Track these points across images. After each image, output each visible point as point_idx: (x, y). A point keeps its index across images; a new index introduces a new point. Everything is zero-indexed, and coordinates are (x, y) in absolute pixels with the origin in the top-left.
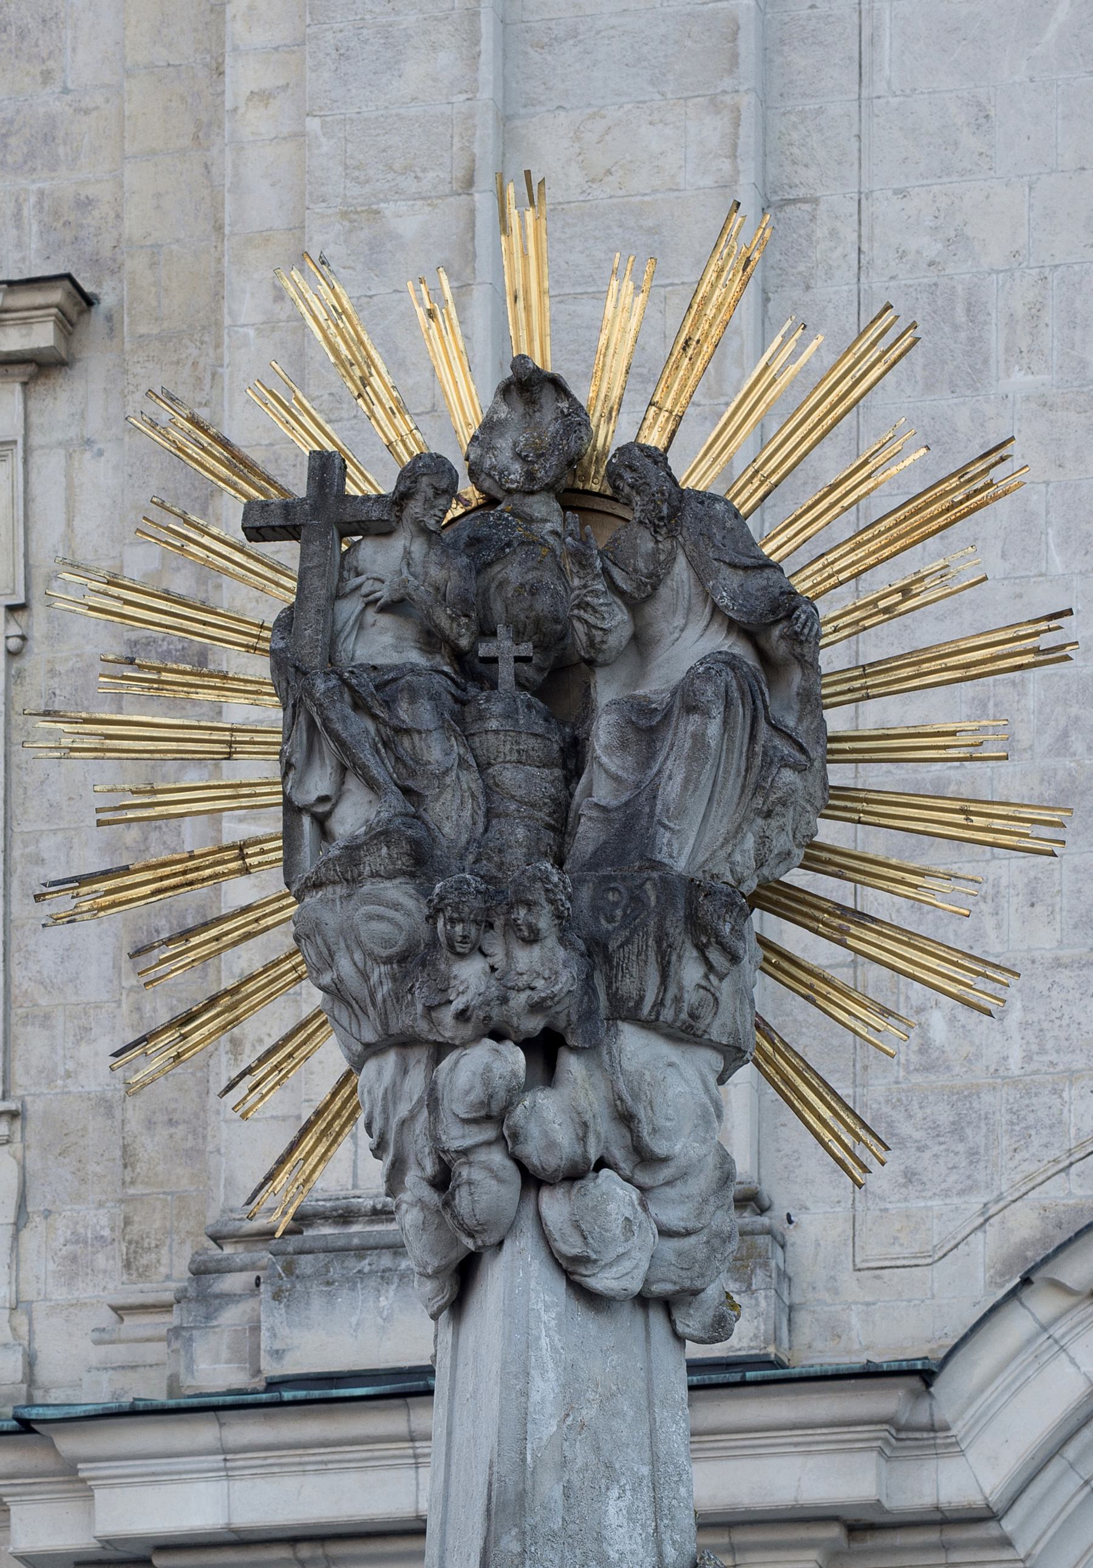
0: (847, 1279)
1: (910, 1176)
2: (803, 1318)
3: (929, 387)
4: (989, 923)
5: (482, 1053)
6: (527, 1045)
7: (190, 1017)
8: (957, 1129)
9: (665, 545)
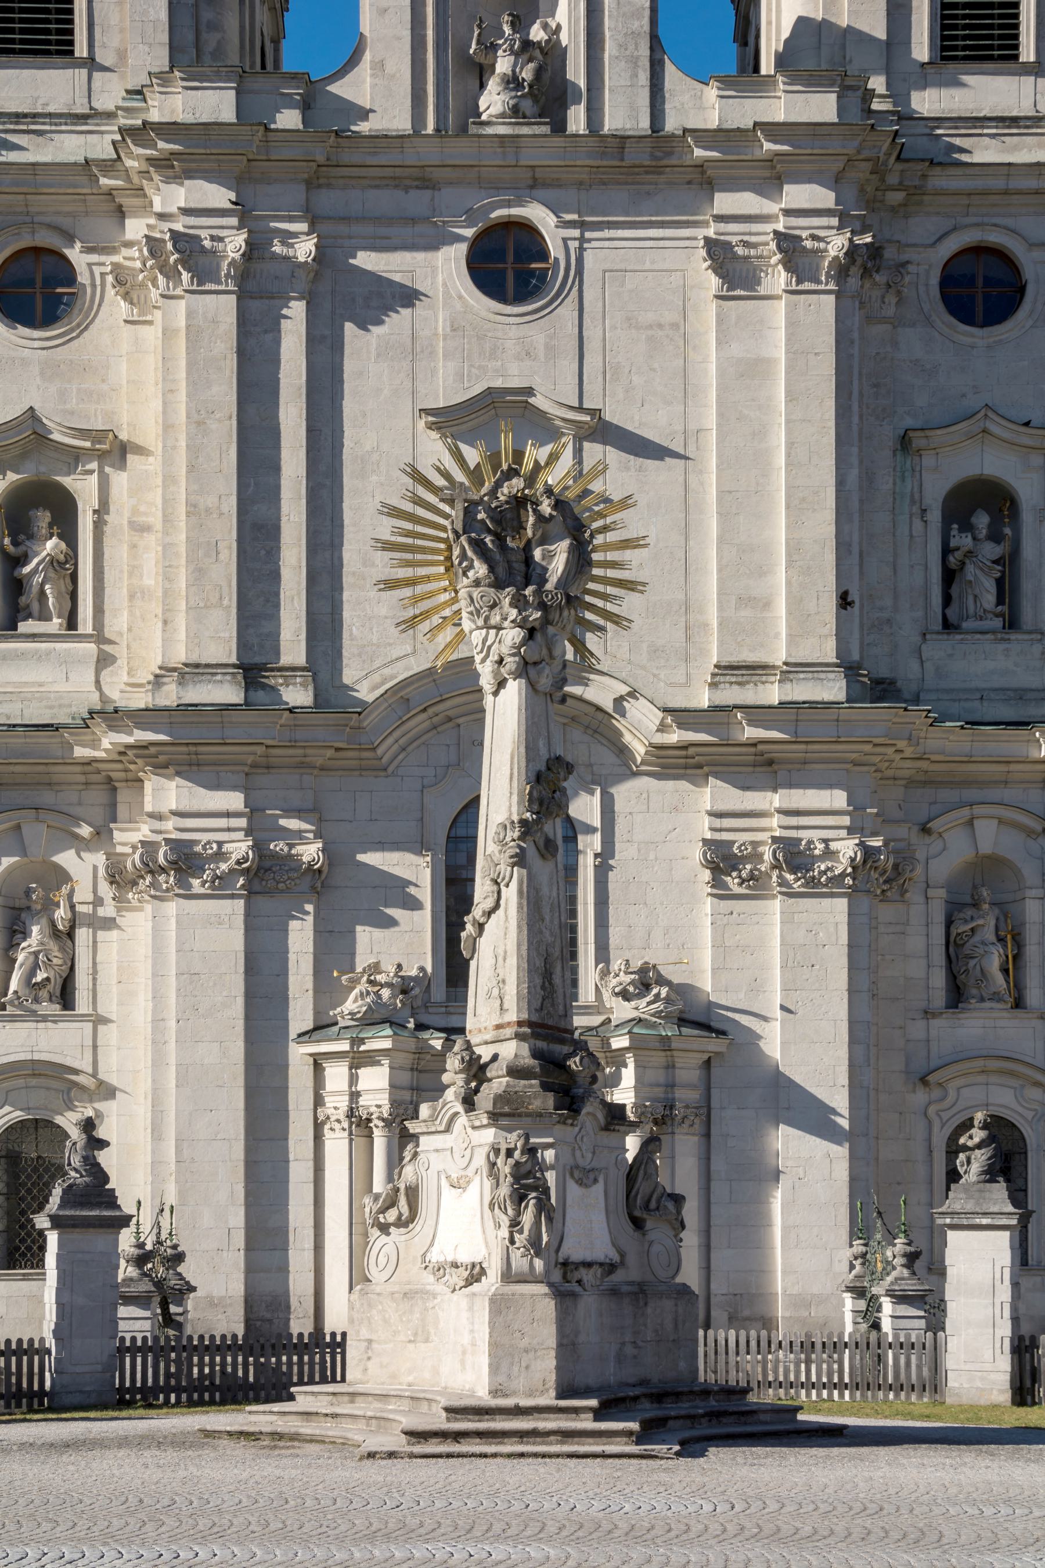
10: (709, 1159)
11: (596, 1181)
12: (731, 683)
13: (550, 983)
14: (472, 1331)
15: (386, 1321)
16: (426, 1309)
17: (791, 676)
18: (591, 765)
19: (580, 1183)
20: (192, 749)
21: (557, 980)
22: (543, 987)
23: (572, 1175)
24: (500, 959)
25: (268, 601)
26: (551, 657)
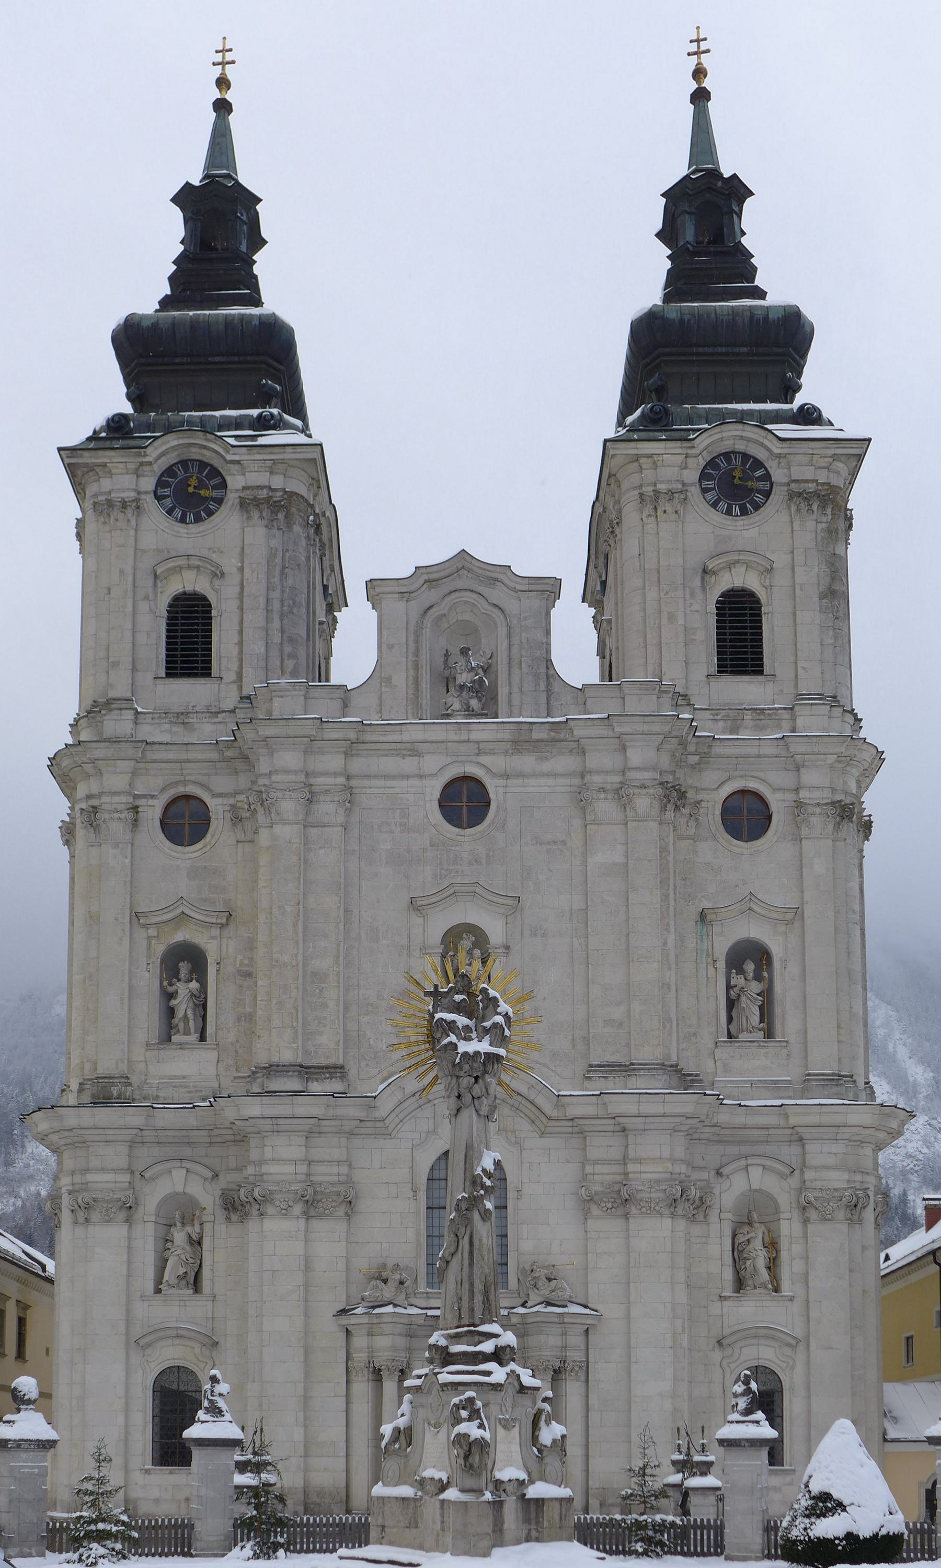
10: (587, 1396)
14: (442, 1522)
18: (515, 1131)
19: (505, 1427)
20: (275, 1121)
21: (492, 1298)
23: (500, 1423)
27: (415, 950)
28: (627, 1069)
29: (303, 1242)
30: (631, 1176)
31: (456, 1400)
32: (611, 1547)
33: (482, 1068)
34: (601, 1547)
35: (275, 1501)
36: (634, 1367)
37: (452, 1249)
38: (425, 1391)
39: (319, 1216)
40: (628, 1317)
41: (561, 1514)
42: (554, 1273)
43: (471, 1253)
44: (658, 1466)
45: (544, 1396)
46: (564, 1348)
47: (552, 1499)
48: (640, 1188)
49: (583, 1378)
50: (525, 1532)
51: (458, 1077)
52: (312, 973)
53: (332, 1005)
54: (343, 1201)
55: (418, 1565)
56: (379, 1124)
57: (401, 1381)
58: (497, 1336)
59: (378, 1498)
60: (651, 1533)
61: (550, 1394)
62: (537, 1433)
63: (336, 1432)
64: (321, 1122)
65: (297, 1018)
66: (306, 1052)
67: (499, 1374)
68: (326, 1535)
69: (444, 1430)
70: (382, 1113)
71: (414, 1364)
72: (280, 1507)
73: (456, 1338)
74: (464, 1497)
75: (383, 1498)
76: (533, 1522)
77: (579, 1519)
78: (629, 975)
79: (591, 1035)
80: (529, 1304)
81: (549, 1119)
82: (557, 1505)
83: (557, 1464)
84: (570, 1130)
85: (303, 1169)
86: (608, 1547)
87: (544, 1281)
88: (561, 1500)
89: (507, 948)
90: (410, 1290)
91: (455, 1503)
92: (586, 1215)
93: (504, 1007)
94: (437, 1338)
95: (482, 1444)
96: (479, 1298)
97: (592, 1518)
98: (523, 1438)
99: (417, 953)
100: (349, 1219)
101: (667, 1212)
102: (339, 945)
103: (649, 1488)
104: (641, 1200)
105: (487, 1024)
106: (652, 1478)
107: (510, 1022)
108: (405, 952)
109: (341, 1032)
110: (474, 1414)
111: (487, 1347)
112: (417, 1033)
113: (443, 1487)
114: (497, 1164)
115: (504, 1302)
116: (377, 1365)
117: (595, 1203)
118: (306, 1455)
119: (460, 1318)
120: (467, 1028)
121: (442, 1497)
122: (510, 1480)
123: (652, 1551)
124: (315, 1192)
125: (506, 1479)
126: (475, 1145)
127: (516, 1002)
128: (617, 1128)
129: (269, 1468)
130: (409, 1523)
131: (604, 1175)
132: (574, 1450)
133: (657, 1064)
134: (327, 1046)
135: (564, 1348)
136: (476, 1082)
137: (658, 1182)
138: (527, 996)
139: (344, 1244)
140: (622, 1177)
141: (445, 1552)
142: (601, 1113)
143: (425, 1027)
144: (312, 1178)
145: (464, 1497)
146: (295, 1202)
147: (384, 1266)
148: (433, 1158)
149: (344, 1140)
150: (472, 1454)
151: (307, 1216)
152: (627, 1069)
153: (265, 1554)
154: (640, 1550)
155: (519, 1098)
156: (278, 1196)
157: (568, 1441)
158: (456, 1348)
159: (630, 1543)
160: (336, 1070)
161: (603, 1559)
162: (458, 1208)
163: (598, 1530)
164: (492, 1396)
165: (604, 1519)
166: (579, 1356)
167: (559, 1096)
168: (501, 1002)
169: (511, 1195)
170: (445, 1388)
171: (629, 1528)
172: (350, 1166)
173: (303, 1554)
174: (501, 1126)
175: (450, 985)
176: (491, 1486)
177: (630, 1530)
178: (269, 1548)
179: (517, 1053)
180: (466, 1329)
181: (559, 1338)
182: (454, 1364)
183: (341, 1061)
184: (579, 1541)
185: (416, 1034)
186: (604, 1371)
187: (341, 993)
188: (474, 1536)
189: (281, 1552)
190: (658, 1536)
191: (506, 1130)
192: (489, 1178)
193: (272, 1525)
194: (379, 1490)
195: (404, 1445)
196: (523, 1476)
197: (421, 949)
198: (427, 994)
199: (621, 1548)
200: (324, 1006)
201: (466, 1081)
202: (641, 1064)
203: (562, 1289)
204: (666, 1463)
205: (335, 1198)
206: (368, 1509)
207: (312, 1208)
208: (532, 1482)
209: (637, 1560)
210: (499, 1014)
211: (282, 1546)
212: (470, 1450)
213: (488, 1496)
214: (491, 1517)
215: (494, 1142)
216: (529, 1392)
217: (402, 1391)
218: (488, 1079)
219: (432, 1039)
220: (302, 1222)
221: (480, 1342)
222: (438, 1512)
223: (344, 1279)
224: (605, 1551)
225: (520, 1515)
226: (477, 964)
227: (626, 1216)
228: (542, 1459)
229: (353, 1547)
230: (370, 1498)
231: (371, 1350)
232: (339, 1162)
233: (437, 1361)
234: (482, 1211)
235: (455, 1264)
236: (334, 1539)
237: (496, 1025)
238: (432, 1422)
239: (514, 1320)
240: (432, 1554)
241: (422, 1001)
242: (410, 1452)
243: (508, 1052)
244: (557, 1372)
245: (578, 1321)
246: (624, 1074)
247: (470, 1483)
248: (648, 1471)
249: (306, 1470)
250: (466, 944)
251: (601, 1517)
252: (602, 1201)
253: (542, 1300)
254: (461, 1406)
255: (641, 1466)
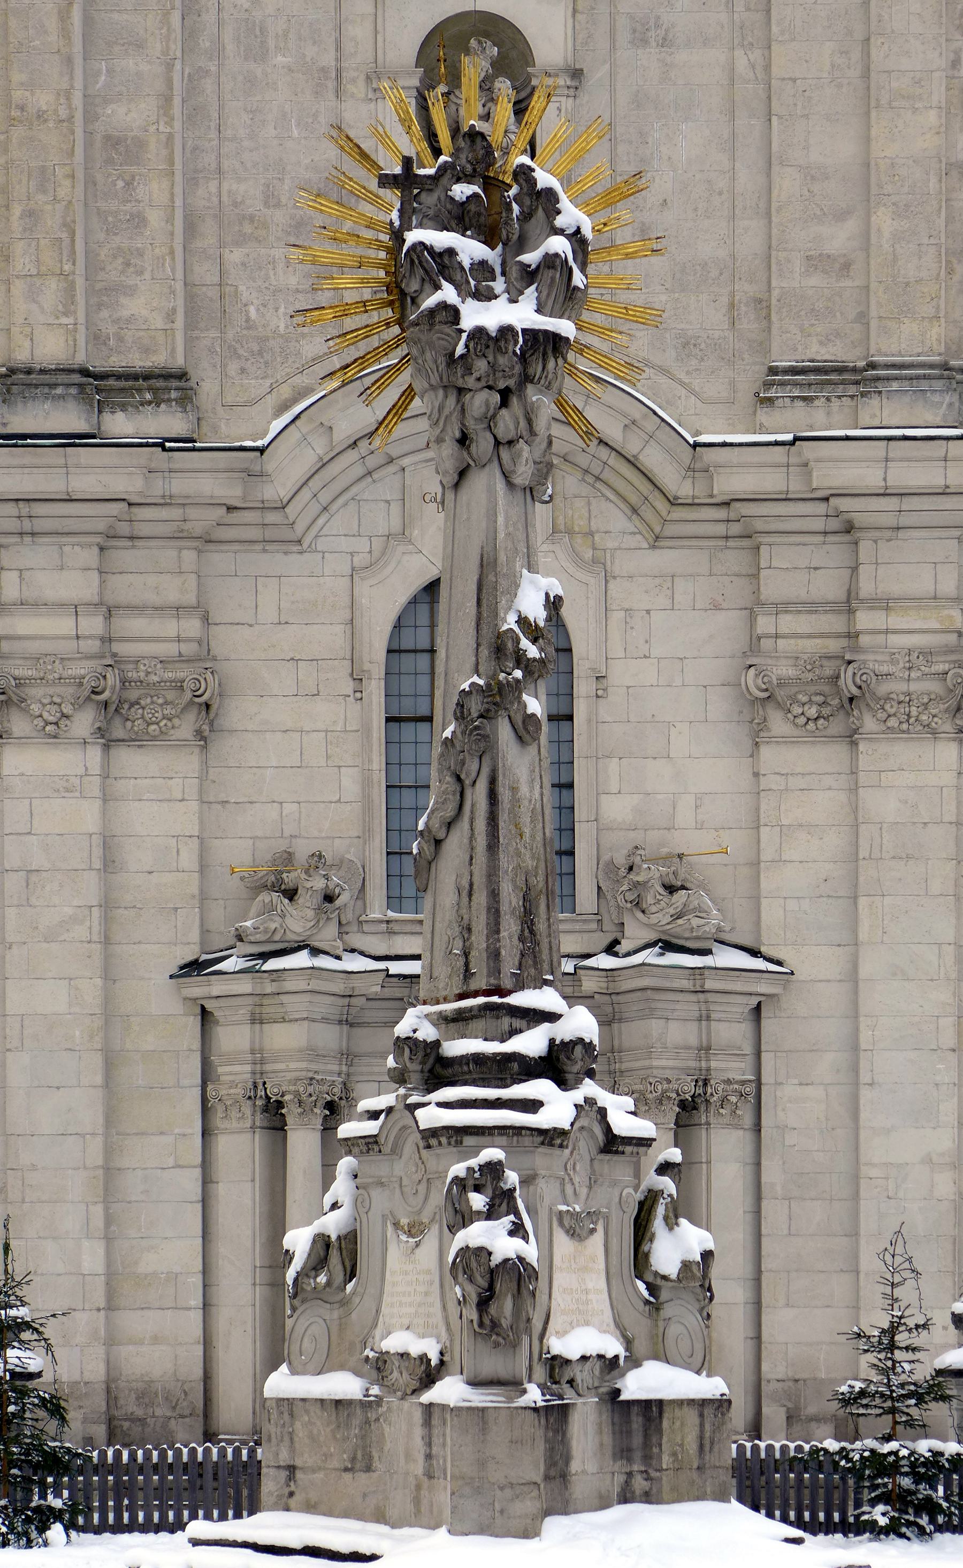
0: (220, 409)
1: (243, 370)
2: (203, 423)
3: (246, 59)
4: (271, 273)
5: (485, 394)
6: (500, 391)
7: (347, 366)
8: (260, 353)
9: (535, 203)
10: (758, 1164)
11: (593, 1231)
12: (793, 398)
13: (532, 932)
14: (429, 1456)
15: (313, 1438)
16: (367, 1422)
17: (881, 386)
18: (591, 534)
19: (572, 1233)
20: (24, 509)
21: (541, 926)
22: (521, 939)
23: (561, 1224)
24: (465, 894)
25: (128, 264)
26: (532, 433)
27: (354, 81)
28: (859, 378)
29: (98, 803)
30: (864, 640)
31: (458, 1169)
32: (814, 1516)
33: (518, 368)
34: (792, 1514)
35: (41, 1413)
36: (866, 1095)
37: (449, 812)
38: (387, 1149)
39: (136, 741)
40: (853, 978)
41: (701, 1438)
42: (682, 875)
43: (493, 820)
44: (925, 1326)
45: (661, 1158)
46: (706, 1049)
47: (680, 1403)
48: (884, 669)
49: (748, 1119)
50: (620, 1479)
51: (461, 391)
52: (107, 138)
53: (155, 218)
54: (191, 703)
55: (373, 1558)
56: (271, 517)
57: (329, 1128)
58: (552, 1017)
59: (280, 1401)
60: (906, 1482)
61: (675, 1155)
62: (645, 1248)
63: (177, 1252)
64: (135, 510)
65: (73, 252)
66: (96, 338)
67: (557, 1107)
68: (161, 1492)
69: (430, 1242)
70: (278, 489)
71: (359, 1088)
72: (52, 1426)
73: (458, 1022)
74: (479, 1398)
75: (290, 1402)
76: (638, 1455)
77: (741, 1448)
78: (868, 140)
79: (775, 293)
80: (624, 946)
81: (673, 502)
82: (691, 1417)
83: (693, 1320)
84: (721, 529)
85: (93, 625)
86: (807, 1515)
87: (657, 887)
88: (702, 1404)
89: (577, 74)
90: (348, 916)
91: (456, 1411)
92: (757, 736)
93: (571, 214)
94: (415, 1023)
95: (519, 1274)
96: (510, 927)
97: (770, 1448)
98: (614, 1260)
99: (359, 89)
100: (205, 747)
101: (948, 727)
102: (170, 67)
103: (903, 1377)
104: (888, 699)
105: (531, 258)
106: (910, 1356)
107: (585, 253)
108: (331, 84)
109: (179, 286)
110: (502, 1203)
111: (531, 1043)
112: (362, 281)
113: (430, 1375)
114: (554, 604)
115: (569, 944)
116: (272, 1091)
117: (779, 705)
118: (111, 1307)
119: (468, 974)
120: (482, 267)
121: (427, 1397)
122: (584, 1358)
123: (909, 1524)
124: (123, 682)
125: (573, 1354)
126: (502, 558)
127: (603, 202)
128: (834, 524)
129: (26, 1335)
130: (350, 1458)
131: (799, 639)
132: (730, 1289)
133: (932, 366)
134: (145, 327)
135: (706, 1049)
136: (504, 403)
137: (927, 654)
138: (627, 188)
139: (194, 806)
140: (844, 642)
141: (435, 1527)
142: (796, 487)
143: (379, 266)
144: (117, 647)
145: (479, 1398)
146: (79, 705)
147: (289, 857)
148: (402, 599)
149: (189, 556)
150: (497, 1296)
151: (107, 741)
152: (859, 378)
153: (19, 1536)
154: (883, 1521)
155: (604, 453)
156: (36, 692)
157: (715, 1271)
158: (457, 1047)
159: (858, 1505)
160: (167, 384)
161: (798, 1541)
162: (461, 714)
163: (785, 1478)
164: (546, 1161)
165: (799, 1449)
166: (739, 1070)
167: (696, 445)
168: (565, 203)
169: (583, 687)
170: (433, 1142)
171: (856, 1472)
172: (206, 619)
173: (107, 1535)
174: (561, 521)
175: (443, 159)
176: (540, 1373)
177: (860, 1477)
178: (28, 1521)
179: (601, 331)
180: (481, 1000)
181: (694, 1026)
182: (452, 1084)
183: (180, 361)
184: (741, 1500)
185: (359, 285)
186: (798, 1105)
187: (178, 190)
188: (502, 1489)
189: (56, 1531)
190: (924, 1490)
191: (570, 532)
192: (534, 641)
193: (36, 1467)
194: (281, 1383)
195: (339, 1277)
196: (613, 1347)
197: (368, 78)
198: (386, 181)
199: (836, 1517)
200: (139, 221)
201: (481, 401)
202: (894, 366)
203: (700, 912)
204: (942, 1319)
205: (171, 695)
206: (256, 1431)
207: (117, 721)
208: (634, 1362)
209: (875, 1545)
210: (560, 232)
211: (57, 1515)
212: (491, 1287)
213: (534, 1395)
214: (541, 1447)
215: (544, 552)
216: (628, 1149)
217: (332, 1150)
218: (533, 395)
219: (399, 297)
220: (95, 754)
221: (513, 1032)
222: (418, 1432)
223: (196, 891)
224: (799, 1523)
225: (608, 1439)
226: (504, 111)
227: (851, 738)
228: (658, 1304)
229: (223, 1517)
230: (260, 1401)
231: (259, 1057)
232: (178, 610)
233: (415, 1078)
234: (518, 719)
235: (455, 846)
236: (179, 1499)
237: (551, 260)
238: (404, 1221)
239: (589, 984)
240: (406, 1531)
241: (375, 200)
242: (354, 1292)
243: (579, 328)
244: (688, 1107)
245: (738, 986)
246: (852, 390)
247: (494, 1364)
248: (902, 1338)
249: (110, 1341)
250: (473, 68)
251: (792, 1446)
252: (794, 700)
253: (653, 936)
254: (470, 1183)
255: (886, 1325)
